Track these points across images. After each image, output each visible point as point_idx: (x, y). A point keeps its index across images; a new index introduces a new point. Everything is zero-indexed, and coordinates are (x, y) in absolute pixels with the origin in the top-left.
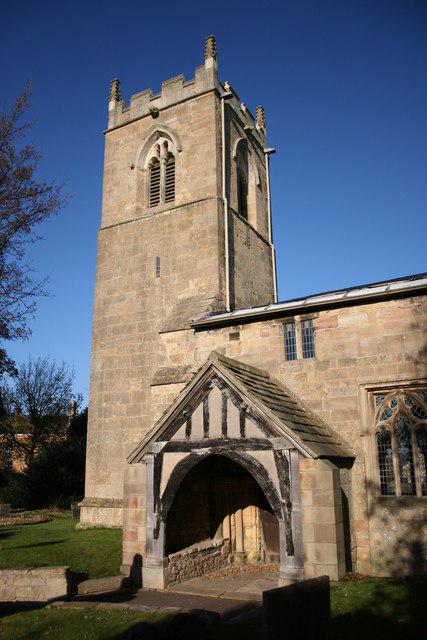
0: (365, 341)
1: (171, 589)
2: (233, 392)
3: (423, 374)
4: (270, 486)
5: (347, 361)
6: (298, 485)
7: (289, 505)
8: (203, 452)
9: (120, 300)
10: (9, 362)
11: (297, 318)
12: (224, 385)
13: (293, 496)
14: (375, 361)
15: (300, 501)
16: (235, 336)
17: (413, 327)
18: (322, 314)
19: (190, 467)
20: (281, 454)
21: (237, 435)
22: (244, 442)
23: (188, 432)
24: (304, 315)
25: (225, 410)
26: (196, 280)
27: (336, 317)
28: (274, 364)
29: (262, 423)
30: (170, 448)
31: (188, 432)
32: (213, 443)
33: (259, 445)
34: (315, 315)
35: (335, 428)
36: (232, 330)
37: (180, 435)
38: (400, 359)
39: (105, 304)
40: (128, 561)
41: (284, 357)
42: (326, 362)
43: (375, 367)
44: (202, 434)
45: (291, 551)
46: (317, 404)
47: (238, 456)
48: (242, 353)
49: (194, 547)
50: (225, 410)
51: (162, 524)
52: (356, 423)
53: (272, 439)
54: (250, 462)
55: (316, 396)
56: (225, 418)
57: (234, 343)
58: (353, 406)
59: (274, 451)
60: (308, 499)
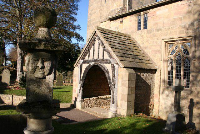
0: (166, 21)
1: (81, 110)
2: (102, 42)
3: (198, 34)
4: (109, 77)
5: (158, 30)
6: (118, 78)
7: (114, 85)
8: (92, 64)
9: (95, 13)
10: (81, 37)
11: (142, 13)
12: (99, 39)
13: (116, 82)
14: (169, 29)
15: (117, 84)
16: (121, 22)
17: (189, 12)
18: (151, 10)
19: (89, 69)
20: (113, 65)
21: (101, 57)
22: (103, 60)
23: (89, 57)
24: (144, 12)
25: (99, 48)
26: (116, 3)
27: (155, 12)
28: (133, 32)
29: (109, 53)
30: (84, 62)
31: (89, 57)
32: (95, 61)
33: (108, 62)
34: (148, 11)
35: (151, 57)
36: (120, 20)
37: (87, 58)
38: (179, 28)
39: (91, 14)
40: (74, 99)
41: (137, 30)
42: (151, 31)
43: (169, 32)
44: (92, 57)
45: (113, 103)
46: (146, 48)
47: (101, 66)
48: (123, 28)
49: (106, 96)
50: (99, 48)
51: (81, 88)
52: (159, 55)
53: (111, 60)
54: (104, 68)
55: (146, 44)
56: (99, 51)
57: (121, 24)
58: (159, 48)
59: (112, 64)
60: (120, 82)
